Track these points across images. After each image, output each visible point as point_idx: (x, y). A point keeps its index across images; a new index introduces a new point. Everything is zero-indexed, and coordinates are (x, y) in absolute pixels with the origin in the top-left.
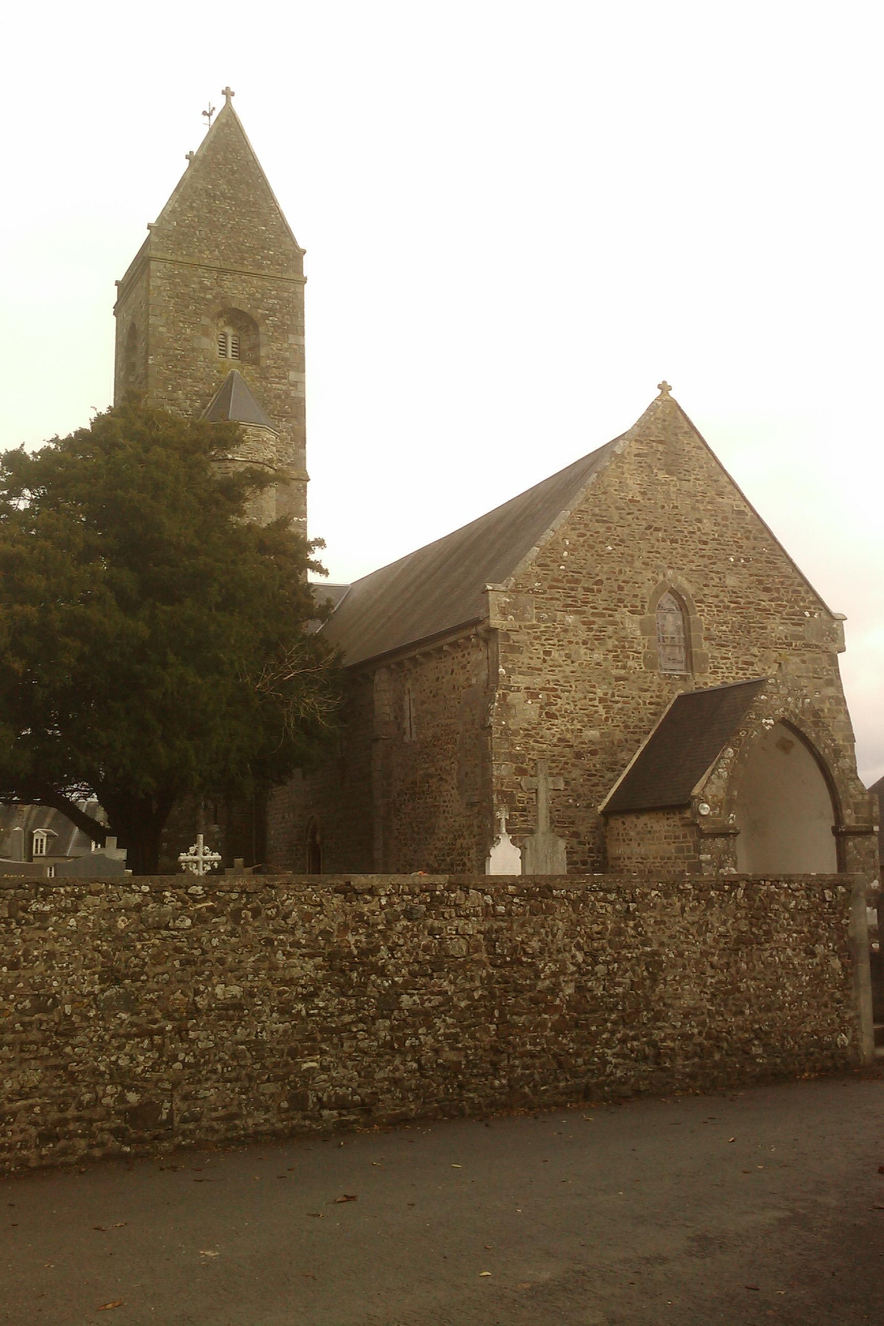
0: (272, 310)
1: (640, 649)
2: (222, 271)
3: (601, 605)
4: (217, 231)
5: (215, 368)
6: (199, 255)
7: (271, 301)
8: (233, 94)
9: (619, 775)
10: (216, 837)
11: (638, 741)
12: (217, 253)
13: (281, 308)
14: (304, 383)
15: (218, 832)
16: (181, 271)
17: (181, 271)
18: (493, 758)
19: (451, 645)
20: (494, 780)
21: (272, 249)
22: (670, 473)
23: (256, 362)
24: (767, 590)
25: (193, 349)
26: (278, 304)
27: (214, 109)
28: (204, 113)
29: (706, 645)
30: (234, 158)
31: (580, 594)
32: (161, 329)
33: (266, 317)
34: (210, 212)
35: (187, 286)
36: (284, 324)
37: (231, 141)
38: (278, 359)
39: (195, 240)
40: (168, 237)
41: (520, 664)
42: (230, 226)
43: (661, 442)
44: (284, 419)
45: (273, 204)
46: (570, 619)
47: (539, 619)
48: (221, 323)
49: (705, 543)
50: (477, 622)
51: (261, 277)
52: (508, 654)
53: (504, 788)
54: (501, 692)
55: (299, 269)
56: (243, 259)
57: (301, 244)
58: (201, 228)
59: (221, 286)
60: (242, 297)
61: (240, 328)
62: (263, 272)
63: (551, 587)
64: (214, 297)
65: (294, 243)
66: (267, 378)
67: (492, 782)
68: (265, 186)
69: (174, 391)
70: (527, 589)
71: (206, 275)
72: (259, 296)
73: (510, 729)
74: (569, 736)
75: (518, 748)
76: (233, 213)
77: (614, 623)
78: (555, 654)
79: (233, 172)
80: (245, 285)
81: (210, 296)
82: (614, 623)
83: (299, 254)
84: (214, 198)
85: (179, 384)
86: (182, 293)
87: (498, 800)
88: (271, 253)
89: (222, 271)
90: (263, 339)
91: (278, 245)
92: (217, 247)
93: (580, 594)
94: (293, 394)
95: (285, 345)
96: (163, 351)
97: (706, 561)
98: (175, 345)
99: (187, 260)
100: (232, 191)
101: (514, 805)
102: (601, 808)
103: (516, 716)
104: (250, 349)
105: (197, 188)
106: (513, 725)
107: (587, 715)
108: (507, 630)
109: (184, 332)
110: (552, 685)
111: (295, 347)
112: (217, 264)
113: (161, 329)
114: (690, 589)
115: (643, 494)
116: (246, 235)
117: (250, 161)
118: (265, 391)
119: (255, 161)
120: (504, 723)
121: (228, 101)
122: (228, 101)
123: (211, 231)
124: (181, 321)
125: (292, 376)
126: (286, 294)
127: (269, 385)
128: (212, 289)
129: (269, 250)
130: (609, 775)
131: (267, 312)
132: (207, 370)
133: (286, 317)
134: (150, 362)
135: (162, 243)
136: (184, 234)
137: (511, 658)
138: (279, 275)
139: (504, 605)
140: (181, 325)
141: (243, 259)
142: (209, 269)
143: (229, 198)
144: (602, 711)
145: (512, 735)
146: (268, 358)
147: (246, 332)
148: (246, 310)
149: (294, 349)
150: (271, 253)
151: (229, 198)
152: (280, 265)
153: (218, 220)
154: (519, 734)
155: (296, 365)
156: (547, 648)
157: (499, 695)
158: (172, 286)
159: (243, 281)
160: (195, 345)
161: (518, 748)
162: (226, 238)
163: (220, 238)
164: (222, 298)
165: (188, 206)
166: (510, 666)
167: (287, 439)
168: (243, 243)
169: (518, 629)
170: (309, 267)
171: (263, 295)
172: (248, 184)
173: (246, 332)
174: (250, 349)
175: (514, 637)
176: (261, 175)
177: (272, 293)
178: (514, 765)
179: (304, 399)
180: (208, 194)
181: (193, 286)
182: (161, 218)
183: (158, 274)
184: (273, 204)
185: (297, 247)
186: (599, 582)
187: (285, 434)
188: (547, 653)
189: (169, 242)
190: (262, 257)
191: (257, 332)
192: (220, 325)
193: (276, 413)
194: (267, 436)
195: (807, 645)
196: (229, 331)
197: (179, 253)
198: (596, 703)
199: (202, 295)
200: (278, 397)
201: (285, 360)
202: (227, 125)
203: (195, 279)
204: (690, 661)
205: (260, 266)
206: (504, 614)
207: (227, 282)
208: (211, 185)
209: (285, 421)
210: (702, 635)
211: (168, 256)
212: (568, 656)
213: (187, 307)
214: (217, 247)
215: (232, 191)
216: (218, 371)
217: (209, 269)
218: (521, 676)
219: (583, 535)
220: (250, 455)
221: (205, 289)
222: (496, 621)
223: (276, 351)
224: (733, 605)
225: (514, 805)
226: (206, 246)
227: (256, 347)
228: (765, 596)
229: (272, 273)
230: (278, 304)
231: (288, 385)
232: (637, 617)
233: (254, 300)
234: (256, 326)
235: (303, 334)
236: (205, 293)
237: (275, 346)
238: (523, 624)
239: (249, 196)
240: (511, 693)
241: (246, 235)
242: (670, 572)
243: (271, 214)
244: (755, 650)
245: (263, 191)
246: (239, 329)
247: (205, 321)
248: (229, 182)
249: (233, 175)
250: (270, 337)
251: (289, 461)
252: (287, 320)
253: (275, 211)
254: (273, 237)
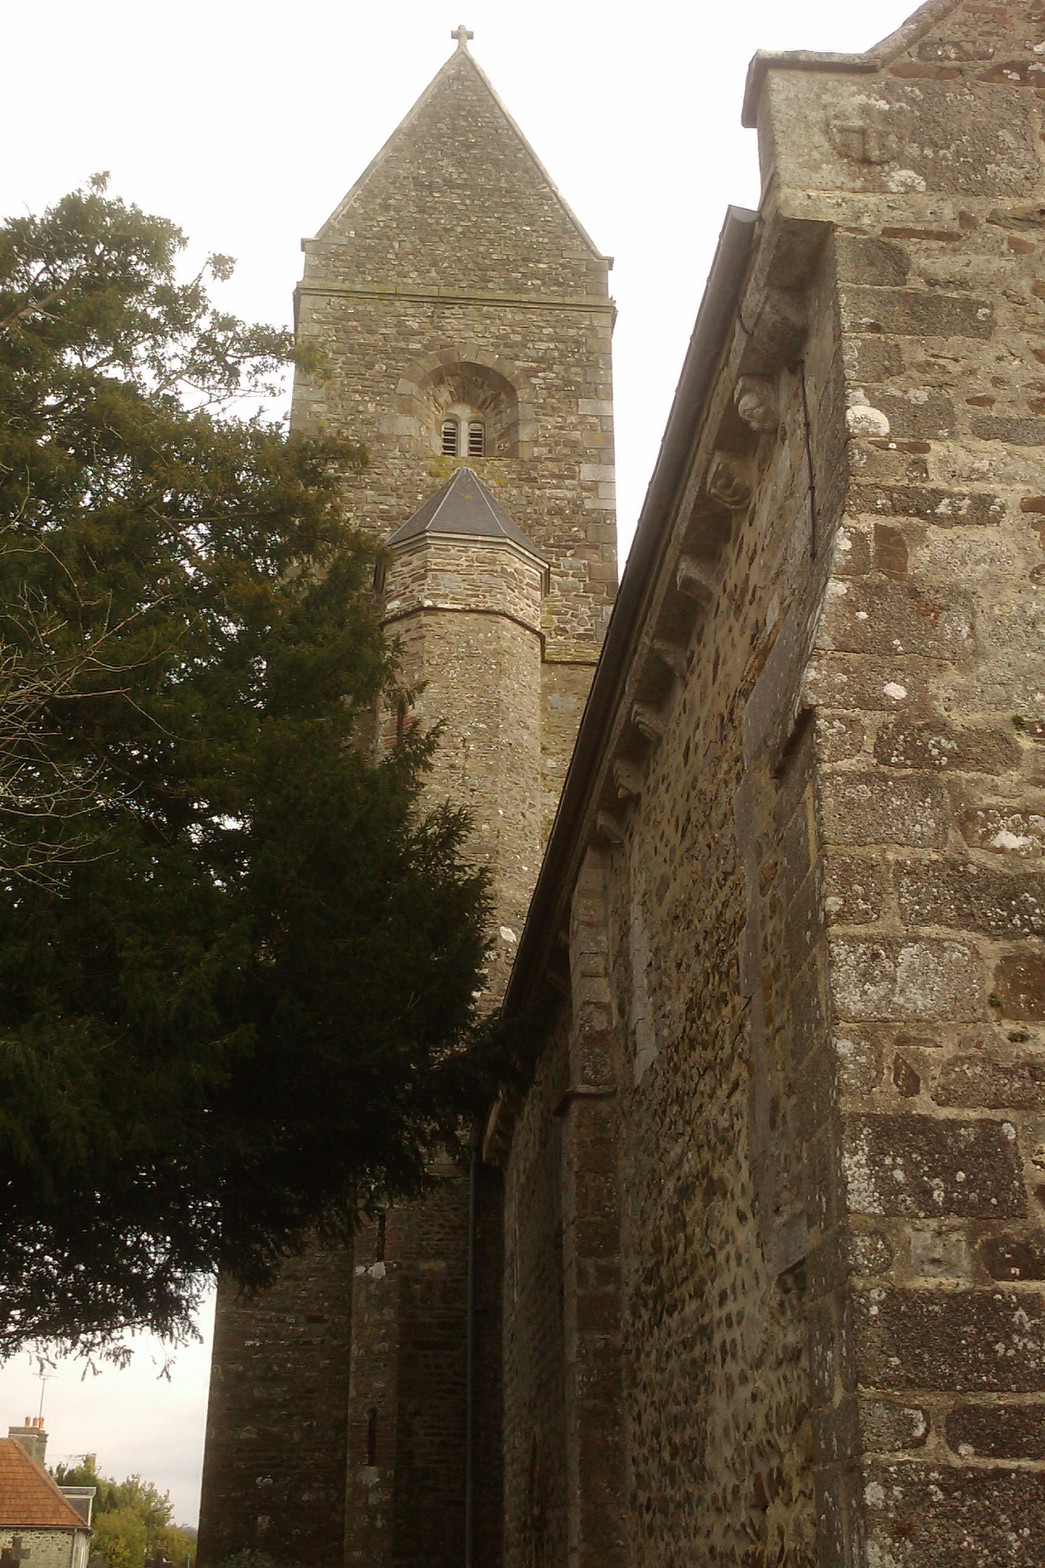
0: (545, 362)
2: (444, 302)
4: (436, 239)
5: (425, 468)
6: (399, 280)
7: (543, 346)
8: (470, 36)
10: (373, 1500)
12: (433, 274)
13: (562, 356)
14: (611, 483)
16: (360, 308)
17: (360, 308)
18: (833, 903)
20: (844, 1047)
21: (545, 260)
25: (380, 438)
26: (556, 348)
30: (470, 125)
32: (315, 407)
33: (533, 373)
34: (422, 211)
35: (371, 332)
37: (466, 100)
38: (557, 444)
39: (390, 256)
40: (336, 255)
41: (981, 386)
42: (460, 229)
44: (568, 554)
45: (547, 189)
48: (445, 397)
51: (523, 306)
52: (904, 340)
53: (923, 1105)
54: (867, 523)
55: (599, 287)
57: (604, 249)
58: (402, 237)
60: (481, 341)
61: (484, 402)
62: (524, 298)
64: (425, 346)
65: (588, 247)
67: (834, 1060)
68: (530, 163)
70: (988, 63)
71: (411, 311)
72: (518, 338)
73: (942, 728)
75: (1008, 840)
76: (467, 209)
79: (469, 147)
80: (488, 322)
81: (418, 346)
83: (600, 266)
84: (431, 188)
86: (360, 345)
87: (886, 1188)
88: (541, 266)
89: (444, 302)
90: (526, 411)
91: (558, 253)
94: (588, 504)
95: (572, 419)
99: (374, 288)
100: (465, 176)
101: (1012, 1229)
103: (978, 653)
105: (397, 177)
106: (963, 697)
108: (886, 232)
109: (361, 408)
111: (591, 420)
116: (491, 242)
117: (502, 128)
118: (530, 503)
119: (511, 126)
120: (896, 691)
123: (422, 241)
124: (356, 392)
125: (587, 472)
126: (572, 332)
127: (537, 492)
128: (423, 334)
131: (533, 364)
132: (408, 472)
133: (573, 370)
135: (327, 266)
136: (369, 248)
137: (921, 357)
138: (559, 300)
139: (857, 123)
140: (357, 397)
142: (416, 300)
143: (459, 186)
145: (958, 759)
146: (536, 442)
147: (495, 408)
149: (592, 425)
150: (541, 266)
151: (459, 186)
152: (560, 285)
153: (438, 223)
154: (1013, 757)
155: (594, 452)
157: (858, 538)
158: (341, 334)
160: (384, 430)
161: (1008, 840)
162: (453, 249)
164: (442, 347)
165: (380, 205)
166: (920, 396)
167: (577, 589)
169: (956, 226)
170: (617, 285)
171: (524, 336)
172: (496, 163)
173: (495, 408)
174: (501, 436)
176: (523, 146)
177: (545, 331)
178: (993, 950)
179: (613, 512)
180: (418, 183)
181: (384, 331)
182: (328, 229)
184: (547, 189)
185: (595, 253)
187: (571, 579)
189: (338, 264)
190: (524, 275)
191: (514, 403)
192: (441, 400)
193: (552, 541)
194: (517, 566)
196: (463, 412)
197: (358, 279)
199: (403, 345)
200: (559, 512)
201: (574, 445)
202: (459, 78)
203: (388, 319)
206: (866, 161)
207: (454, 321)
208: (425, 169)
209: (572, 556)
211: (337, 285)
213: (370, 366)
214: (435, 264)
215: (465, 176)
216: (430, 474)
217: (416, 300)
218: (995, 445)
220: (474, 599)
221: (407, 334)
223: (553, 431)
225: (1012, 1229)
226: (413, 265)
229: (543, 298)
230: (556, 348)
231: (579, 490)
233: (506, 346)
235: (609, 397)
236: (405, 340)
237: (550, 422)
238: (979, 207)
239: (498, 180)
240: (935, 533)
241: (491, 242)
243: (542, 204)
245: (526, 171)
246: (481, 407)
247: (405, 387)
248: (460, 163)
249: (467, 151)
250: (540, 406)
251: (581, 630)
252: (576, 374)
253: (552, 199)
254: (546, 240)
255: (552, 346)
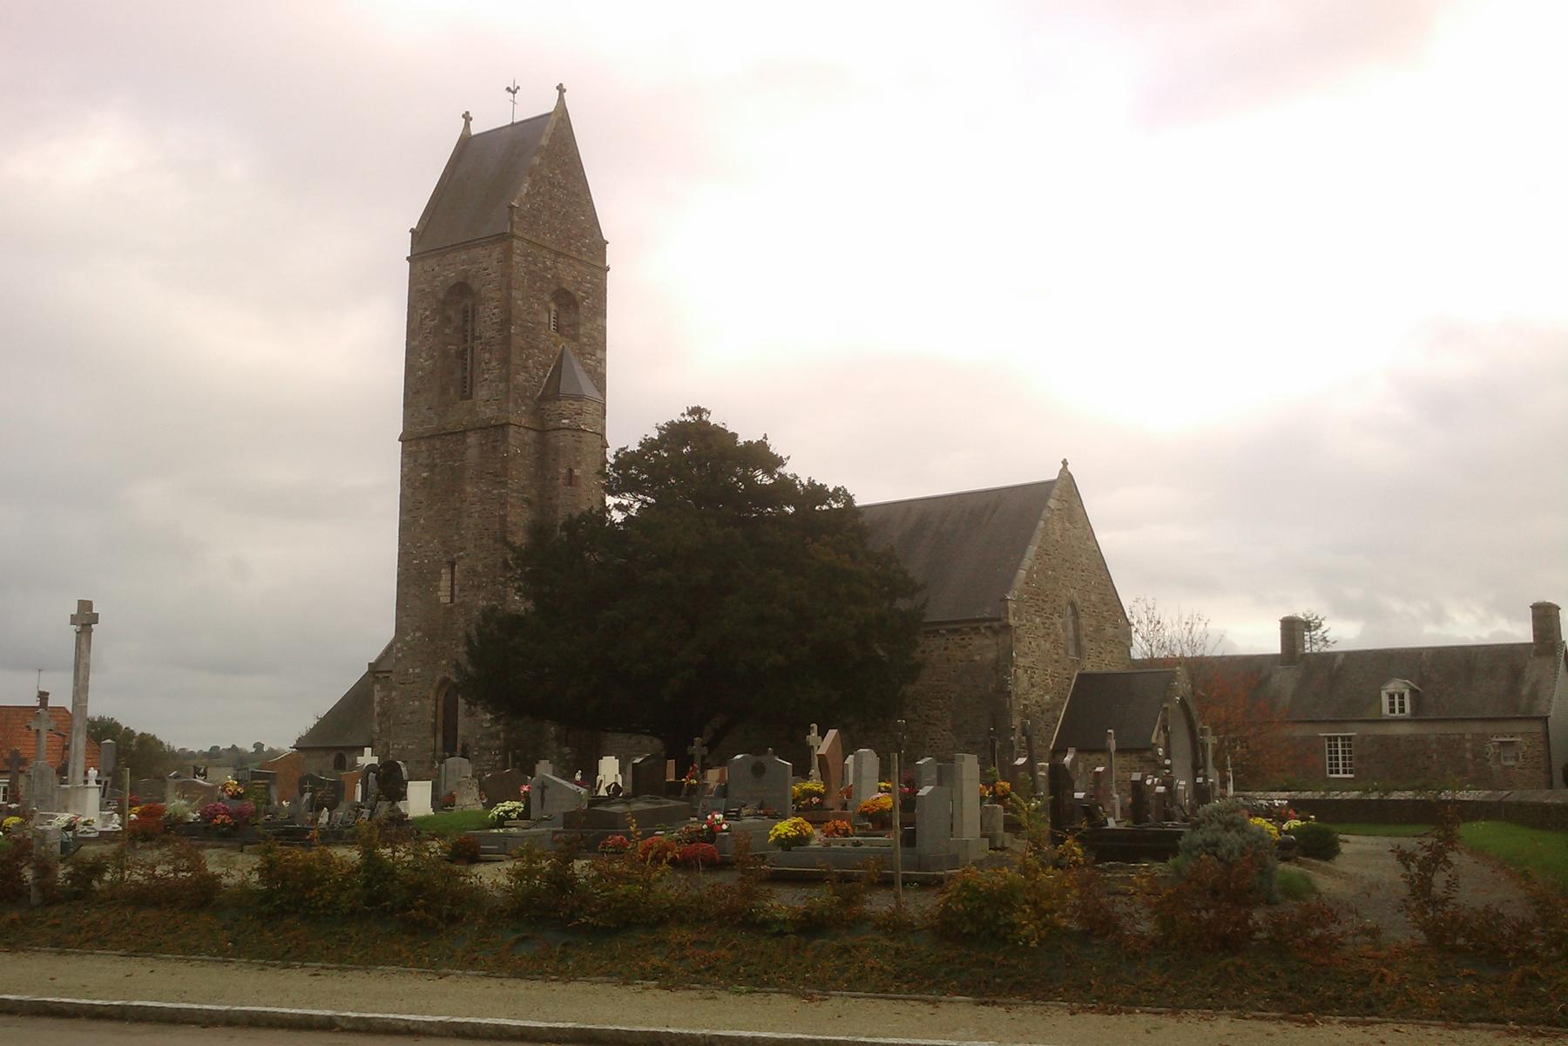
1: (1062, 641)
2: (558, 254)
3: (1048, 611)
9: (1056, 726)
11: (1063, 703)
15: (569, 754)
19: (948, 631)
22: (1070, 523)
23: (575, 338)
24: (1105, 604)
25: (539, 323)
27: (518, 88)
28: (508, 89)
29: (1085, 638)
31: (1040, 603)
32: (520, 302)
33: (584, 299)
36: (594, 307)
43: (1066, 501)
46: (1038, 620)
47: (1027, 619)
49: (1083, 571)
50: (999, 620)
56: (570, 244)
59: (556, 268)
63: (1031, 598)
66: (583, 354)
69: (527, 360)
72: (579, 279)
74: (1039, 699)
77: (1053, 624)
78: (1033, 644)
79: (566, 164)
81: (549, 276)
82: (1053, 624)
83: (603, 244)
84: (552, 184)
85: (530, 353)
92: (555, 231)
93: (1040, 603)
96: (519, 322)
97: (1083, 584)
98: (528, 318)
102: (1051, 747)
104: (569, 326)
107: (1045, 685)
110: (1032, 665)
112: (553, 247)
113: (520, 302)
114: (1079, 602)
115: (1061, 536)
121: (561, 98)
122: (561, 98)
125: (599, 352)
126: (596, 280)
129: (586, 238)
130: (1054, 725)
134: (512, 331)
140: (532, 299)
141: (570, 244)
142: (550, 251)
144: (1051, 683)
148: (572, 292)
156: (1031, 640)
159: (570, 265)
163: (557, 223)
168: (570, 230)
170: (612, 257)
174: (569, 326)
175: (1018, 631)
183: (518, 251)
186: (1047, 596)
188: (1030, 643)
195: (1120, 642)
198: (1048, 677)
199: (545, 274)
201: (594, 338)
204: (1079, 650)
205: (579, 251)
210: (1084, 633)
212: (1037, 645)
217: (550, 251)
219: (1040, 564)
221: (547, 269)
222: (1012, 621)
224: (1094, 614)
227: (575, 325)
228: (1105, 608)
232: (1061, 620)
234: (577, 307)
237: (589, 325)
242: (1072, 590)
244: (1102, 645)
255: (589, 285)
